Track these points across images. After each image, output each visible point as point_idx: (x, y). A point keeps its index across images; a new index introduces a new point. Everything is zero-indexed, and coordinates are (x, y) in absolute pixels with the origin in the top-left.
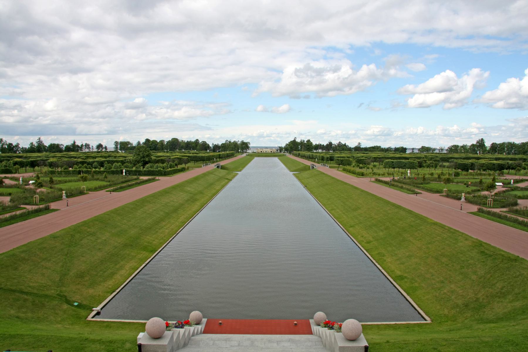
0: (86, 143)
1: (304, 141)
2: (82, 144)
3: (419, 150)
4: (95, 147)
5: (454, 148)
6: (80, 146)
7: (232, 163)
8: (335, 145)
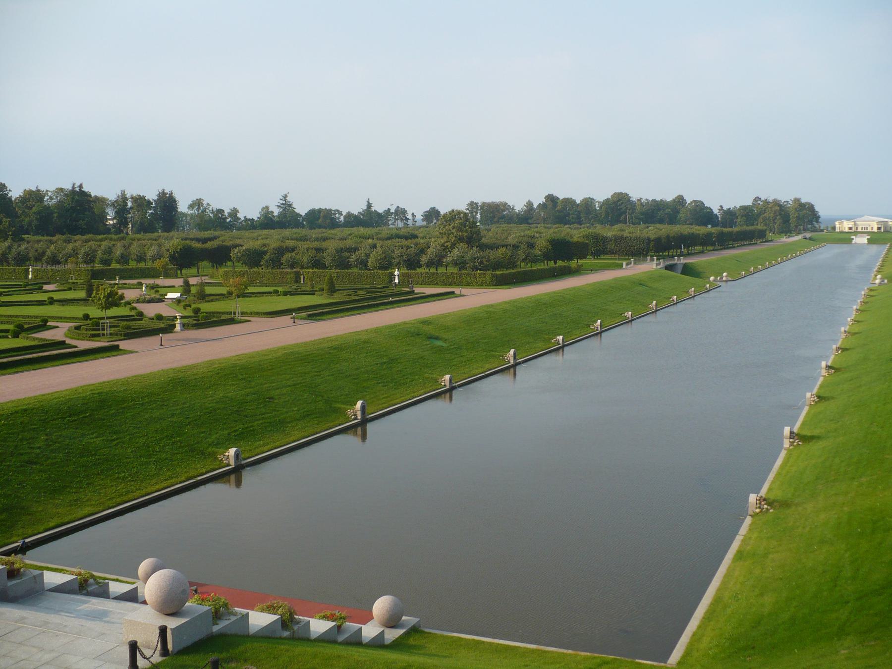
0: (398, 207)
4: (419, 217)
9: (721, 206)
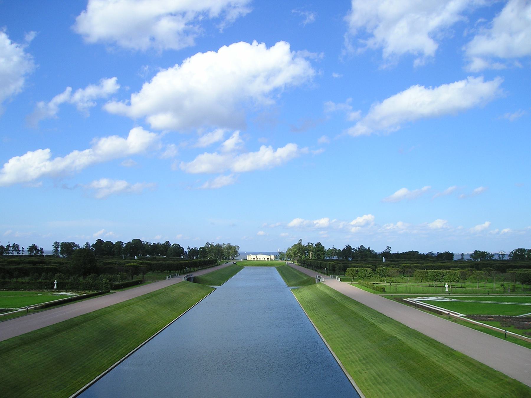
0: (14, 244)
1: (312, 245)
2: (8, 245)
3: (471, 256)
4: (26, 249)
5: (519, 252)
6: (6, 248)
7: (208, 275)
8: (356, 250)
9: (189, 247)
